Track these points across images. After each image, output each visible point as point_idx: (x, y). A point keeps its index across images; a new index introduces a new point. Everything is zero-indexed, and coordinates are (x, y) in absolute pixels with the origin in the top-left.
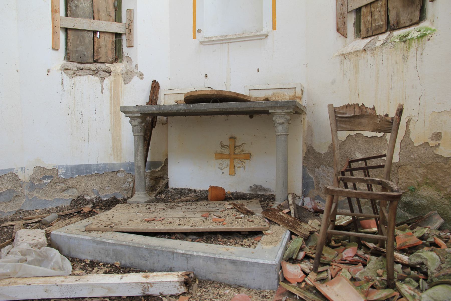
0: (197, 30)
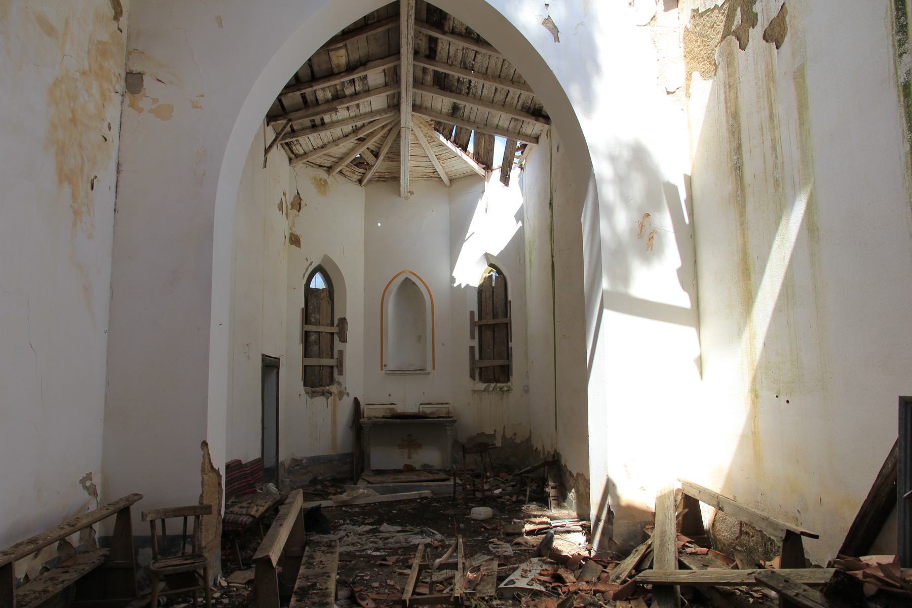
0: (384, 364)
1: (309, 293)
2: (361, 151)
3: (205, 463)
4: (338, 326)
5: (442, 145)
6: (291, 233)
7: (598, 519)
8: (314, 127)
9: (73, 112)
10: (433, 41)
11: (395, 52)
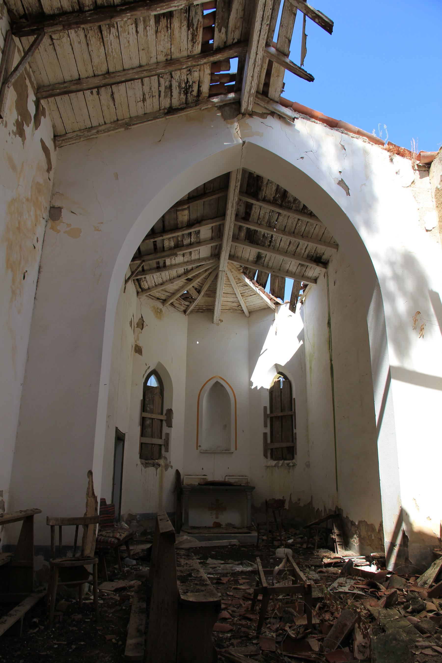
0: (199, 445)
1: (147, 389)
2: (188, 288)
3: (89, 488)
4: (166, 415)
5: (246, 285)
6: (136, 345)
7: (393, 544)
8: (159, 268)
9: (19, 223)
10: (249, 207)
11: (222, 215)
